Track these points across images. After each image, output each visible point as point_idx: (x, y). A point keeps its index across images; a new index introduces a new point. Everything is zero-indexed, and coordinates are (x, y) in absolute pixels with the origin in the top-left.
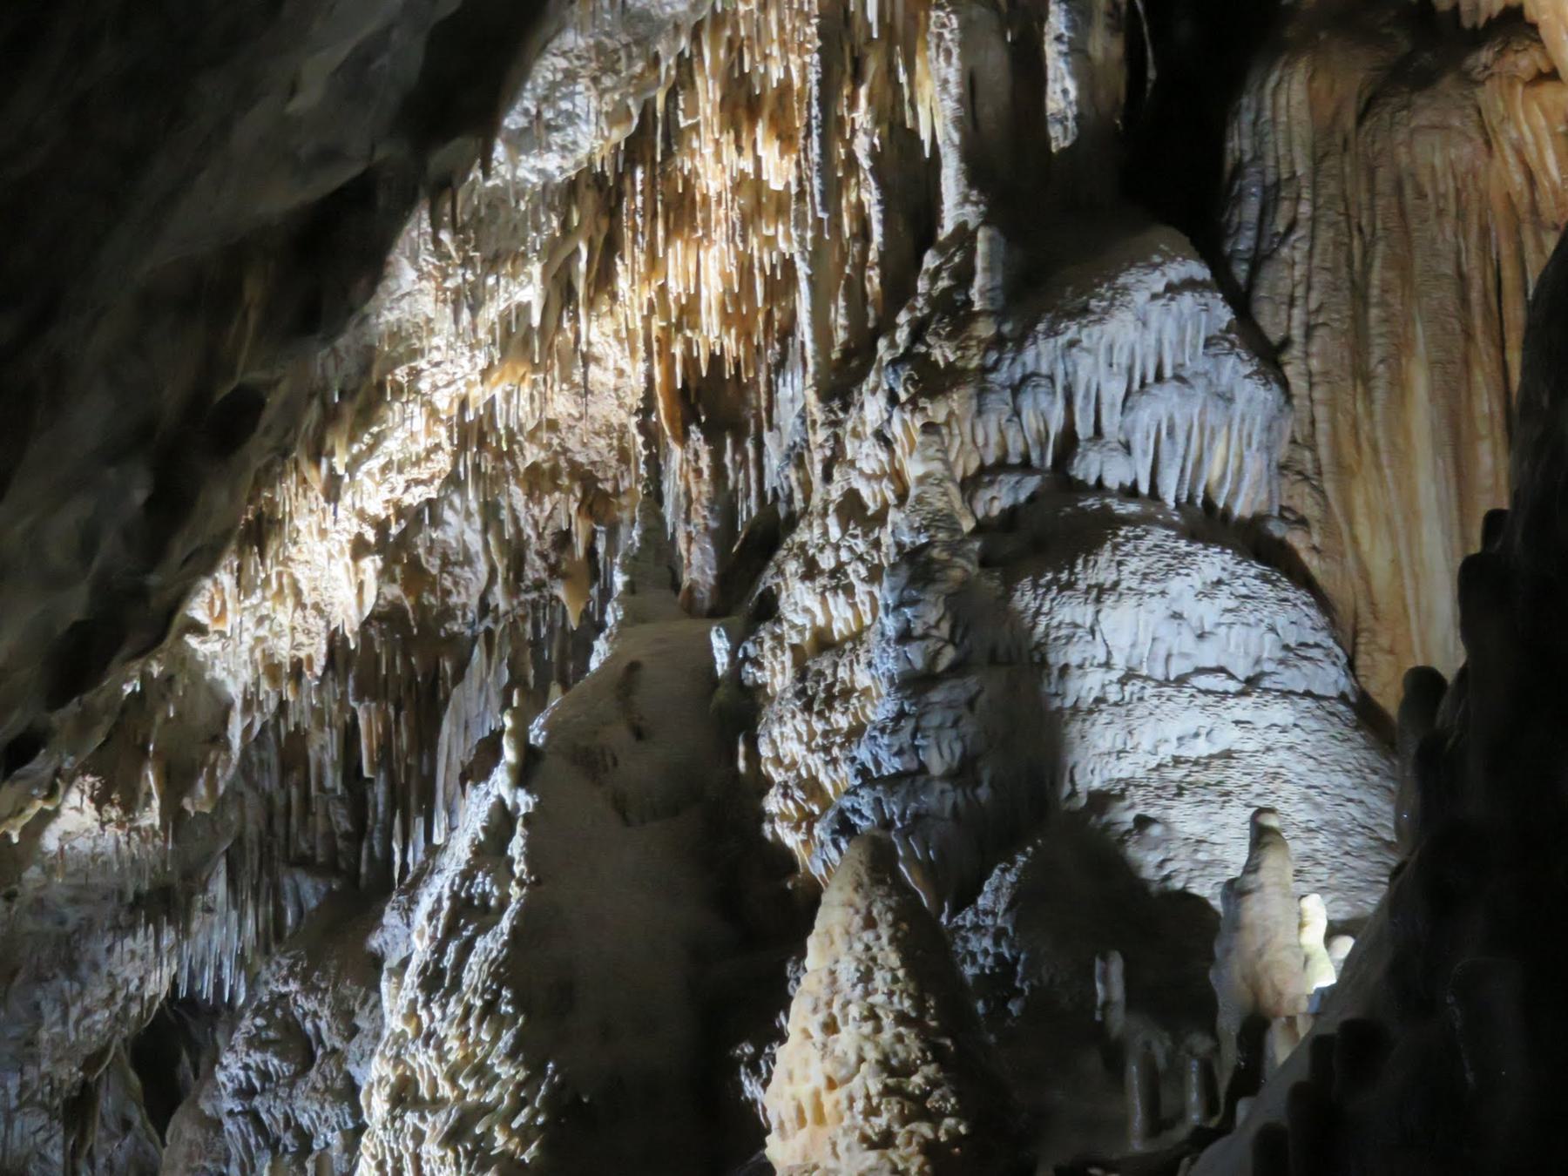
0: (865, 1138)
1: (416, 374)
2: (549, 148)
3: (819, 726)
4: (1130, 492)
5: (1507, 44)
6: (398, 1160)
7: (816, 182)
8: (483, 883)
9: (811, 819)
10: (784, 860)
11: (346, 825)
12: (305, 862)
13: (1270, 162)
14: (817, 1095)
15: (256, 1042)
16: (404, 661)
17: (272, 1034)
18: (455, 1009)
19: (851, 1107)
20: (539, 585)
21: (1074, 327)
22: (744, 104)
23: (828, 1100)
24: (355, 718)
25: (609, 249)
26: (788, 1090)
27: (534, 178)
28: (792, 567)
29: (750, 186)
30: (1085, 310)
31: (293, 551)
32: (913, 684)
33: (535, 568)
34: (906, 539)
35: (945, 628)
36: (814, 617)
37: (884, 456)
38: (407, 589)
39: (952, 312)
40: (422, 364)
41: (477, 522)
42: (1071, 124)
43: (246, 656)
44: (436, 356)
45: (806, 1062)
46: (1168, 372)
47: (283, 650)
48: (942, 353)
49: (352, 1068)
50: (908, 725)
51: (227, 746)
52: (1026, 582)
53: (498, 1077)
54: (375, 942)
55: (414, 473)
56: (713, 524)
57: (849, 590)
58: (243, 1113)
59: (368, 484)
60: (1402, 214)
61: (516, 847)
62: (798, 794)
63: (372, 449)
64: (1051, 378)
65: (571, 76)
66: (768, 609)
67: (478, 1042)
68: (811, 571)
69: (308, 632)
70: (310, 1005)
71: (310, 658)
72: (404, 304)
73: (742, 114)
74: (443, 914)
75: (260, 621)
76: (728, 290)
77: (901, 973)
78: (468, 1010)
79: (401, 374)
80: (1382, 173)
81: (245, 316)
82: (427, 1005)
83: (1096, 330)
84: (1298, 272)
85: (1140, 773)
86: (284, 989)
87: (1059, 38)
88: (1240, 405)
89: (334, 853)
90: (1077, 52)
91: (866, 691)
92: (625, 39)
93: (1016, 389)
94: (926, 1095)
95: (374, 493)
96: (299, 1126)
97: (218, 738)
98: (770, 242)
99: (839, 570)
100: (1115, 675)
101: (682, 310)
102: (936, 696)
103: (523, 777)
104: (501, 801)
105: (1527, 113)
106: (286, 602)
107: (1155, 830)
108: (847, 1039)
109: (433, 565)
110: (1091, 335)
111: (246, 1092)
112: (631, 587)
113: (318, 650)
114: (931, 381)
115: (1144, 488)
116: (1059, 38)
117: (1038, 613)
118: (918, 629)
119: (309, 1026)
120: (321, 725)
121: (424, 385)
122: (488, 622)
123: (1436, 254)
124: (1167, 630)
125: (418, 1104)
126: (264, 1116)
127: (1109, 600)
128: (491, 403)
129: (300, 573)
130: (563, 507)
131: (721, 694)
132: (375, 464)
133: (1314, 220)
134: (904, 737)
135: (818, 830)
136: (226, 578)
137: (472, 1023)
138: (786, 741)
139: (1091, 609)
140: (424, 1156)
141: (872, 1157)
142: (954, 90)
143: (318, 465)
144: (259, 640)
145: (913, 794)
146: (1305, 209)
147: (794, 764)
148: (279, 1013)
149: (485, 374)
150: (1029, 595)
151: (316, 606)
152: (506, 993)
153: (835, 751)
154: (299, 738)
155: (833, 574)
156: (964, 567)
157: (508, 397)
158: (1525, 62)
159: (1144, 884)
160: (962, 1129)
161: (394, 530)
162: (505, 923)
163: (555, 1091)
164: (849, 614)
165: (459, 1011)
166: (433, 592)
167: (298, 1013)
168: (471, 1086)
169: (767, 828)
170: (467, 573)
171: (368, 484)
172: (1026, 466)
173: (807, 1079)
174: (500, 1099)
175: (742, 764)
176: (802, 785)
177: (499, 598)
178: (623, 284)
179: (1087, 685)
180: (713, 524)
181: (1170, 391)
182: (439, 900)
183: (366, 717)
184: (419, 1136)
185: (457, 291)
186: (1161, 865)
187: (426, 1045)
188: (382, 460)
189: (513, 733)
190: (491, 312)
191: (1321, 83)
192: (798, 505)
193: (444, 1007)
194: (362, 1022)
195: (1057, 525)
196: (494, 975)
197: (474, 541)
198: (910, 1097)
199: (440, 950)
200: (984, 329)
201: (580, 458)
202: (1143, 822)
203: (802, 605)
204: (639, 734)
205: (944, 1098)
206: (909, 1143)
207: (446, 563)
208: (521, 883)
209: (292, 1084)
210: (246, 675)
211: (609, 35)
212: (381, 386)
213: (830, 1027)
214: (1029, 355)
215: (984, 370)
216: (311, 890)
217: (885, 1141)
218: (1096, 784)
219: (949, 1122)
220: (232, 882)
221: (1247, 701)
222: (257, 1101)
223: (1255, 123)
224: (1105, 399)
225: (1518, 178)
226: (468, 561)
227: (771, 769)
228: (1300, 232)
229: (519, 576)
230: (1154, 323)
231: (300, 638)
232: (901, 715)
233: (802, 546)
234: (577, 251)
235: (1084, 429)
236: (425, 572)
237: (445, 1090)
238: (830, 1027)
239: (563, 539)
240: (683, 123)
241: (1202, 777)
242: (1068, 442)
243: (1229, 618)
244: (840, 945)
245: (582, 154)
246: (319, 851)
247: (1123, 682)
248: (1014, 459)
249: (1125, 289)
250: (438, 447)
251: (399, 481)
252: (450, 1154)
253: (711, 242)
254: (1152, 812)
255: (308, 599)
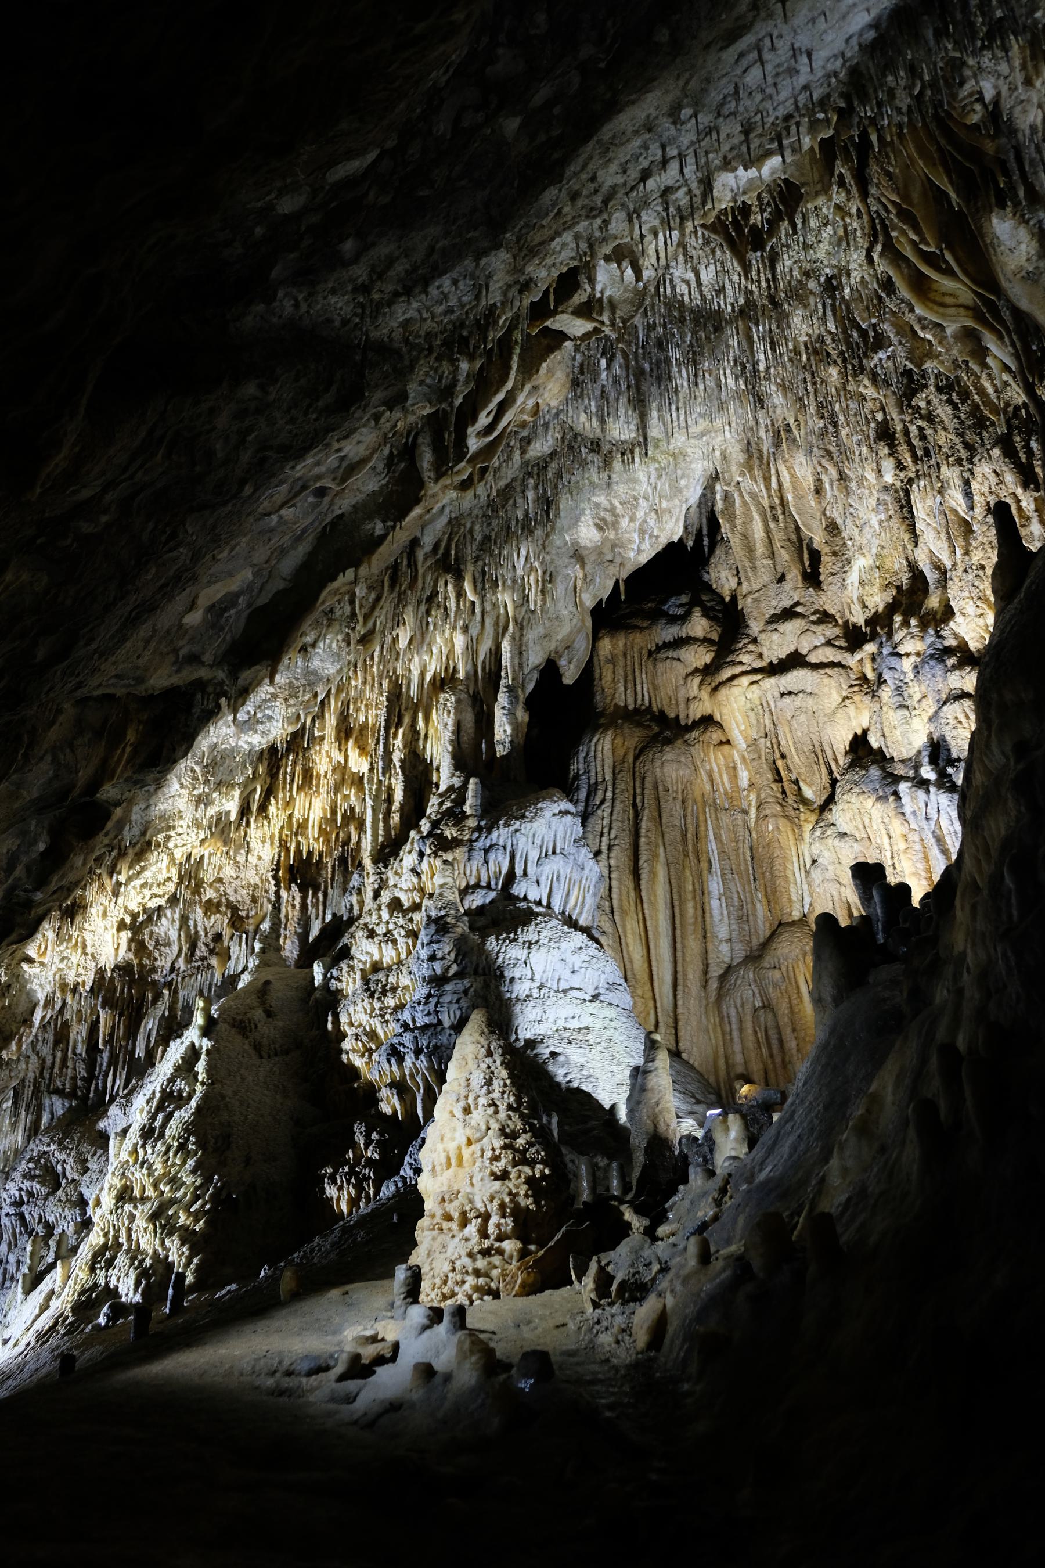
0: (493, 1174)
1: (168, 838)
2: (256, 732)
3: (377, 1005)
4: (539, 903)
5: (706, 729)
6: (117, 1231)
7: (381, 764)
8: (180, 1084)
9: (371, 1052)
10: (353, 1072)
11: (84, 1073)
12: (60, 1092)
13: (593, 774)
14: (459, 1149)
15: (27, 1176)
16: (130, 991)
17: (37, 1172)
18: (160, 1147)
19: (482, 1156)
20: (203, 959)
21: (518, 823)
22: (345, 731)
23: (466, 1153)
24: (98, 1017)
25: (269, 793)
26: (440, 1147)
27: (246, 746)
28: (360, 934)
29: (342, 769)
30: (523, 816)
31: (86, 925)
32: (437, 981)
33: (201, 950)
34: (433, 914)
35: (453, 955)
36: (372, 955)
37: (415, 880)
38: (136, 955)
39: (456, 816)
40: (172, 833)
41: (177, 925)
42: (507, 745)
43: (51, 978)
44: (179, 830)
45: (455, 1129)
46: (558, 851)
47: (71, 978)
48: (450, 832)
49: (84, 1190)
50: (433, 1001)
51: (31, 1026)
52: (493, 938)
53: (184, 1183)
54: (102, 1125)
55: (156, 890)
56: (299, 930)
57: (395, 942)
58: (15, 1215)
59: (133, 893)
60: (658, 799)
61: (201, 1067)
62: (364, 1038)
63: (139, 873)
64: (504, 847)
65: (274, 697)
66: (346, 953)
67: (174, 1164)
68: (372, 934)
69: (85, 968)
70: (63, 1156)
71: (84, 982)
72: (170, 801)
73: (343, 735)
74: (155, 1101)
75: (63, 959)
76: (324, 818)
77: (508, 1082)
78: (169, 1148)
79: (160, 837)
80: (647, 779)
81: (124, 749)
82: (143, 1146)
83: (529, 825)
84: (606, 821)
85: (549, 1033)
86: (46, 1149)
87: (504, 708)
88: (586, 872)
89: (74, 1087)
90: (511, 714)
91: (406, 987)
92: (303, 682)
93: (486, 851)
94: (526, 1150)
95: (134, 898)
96: (47, 1222)
97: (27, 1022)
98: (346, 797)
99: (388, 933)
100: (537, 984)
101: (299, 826)
102: (448, 987)
103: (206, 1031)
104: (193, 1044)
105: (716, 758)
106: (72, 955)
107: (561, 1058)
108: (478, 1117)
109: (150, 945)
110: (526, 827)
111: (18, 1203)
112: (263, 950)
113: (89, 978)
114: (443, 845)
115: (545, 903)
116: (504, 708)
117: (498, 952)
118: (439, 955)
119: (59, 1167)
120: (80, 1020)
121: (171, 845)
122: (173, 976)
123: (672, 816)
124: (559, 966)
125: (132, 1200)
126: (27, 1216)
127: (534, 948)
128: (202, 857)
129: (88, 936)
130: (220, 922)
131: (318, 994)
132: (137, 883)
133: (613, 799)
134: (431, 1006)
135: (375, 1056)
136: (51, 935)
137: (171, 1154)
138: (357, 1015)
139: (526, 951)
140: (134, 1228)
141: (498, 1184)
142: (450, 728)
143: (111, 877)
144: (60, 970)
145: (435, 1034)
146: (609, 794)
147: (360, 1025)
148: (42, 1161)
149: (203, 841)
150: (494, 943)
151: (93, 955)
152: (192, 1139)
153: (387, 1017)
154: (66, 1025)
155: (385, 935)
156: (463, 927)
157: (210, 855)
158: (716, 736)
159: (559, 1084)
160: (547, 1171)
161: (140, 919)
162: (193, 1103)
163: (217, 1192)
164: (394, 954)
165: (164, 1149)
166: (149, 958)
167: (54, 1161)
168: (167, 1188)
169: (344, 1057)
170: (167, 950)
171: (133, 893)
172: (488, 887)
173: (453, 1139)
174: (185, 1194)
175: (330, 1026)
176: (366, 1034)
177: (181, 964)
178: (272, 809)
179: (521, 989)
180: (299, 930)
181: (559, 858)
182: (154, 1093)
183: (104, 1016)
184: (132, 1217)
185: (200, 796)
186: (565, 1075)
187: (142, 1167)
188: (142, 881)
189: (203, 1009)
190: (212, 811)
191: (619, 740)
192: (356, 912)
193: (154, 1147)
194: (92, 1165)
195: (507, 914)
196: (186, 1130)
197: (173, 934)
198: (516, 1150)
199: (153, 1118)
200: (472, 823)
201: (232, 899)
202: (554, 1055)
203: (365, 950)
204: (269, 1014)
205: (538, 1152)
206: (519, 1177)
207: (157, 944)
208: (203, 1084)
209: (46, 1199)
210: (49, 988)
211: (297, 679)
212: (149, 843)
213: (467, 1110)
214: (495, 835)
215: (471, 841)
216: (60, 1106)
217: (504, 1176)
218: (528, 1036)
219: (539, 1167)
220: (15, 1104)
221: (594, 1004)
222: (24, 1208)
223: (585, 758)
224: (530, 859)
225: (708, 787)
226: (168, 944)
227: (347, 1028)
228: (608, 804)
229: (193, 954)
230: (553, 828)
231: (81, 971)
232: (429, 996)
233: (366, 924)
234: (255, 789)
235: (519, 871)
236: (146, 948)
237: (150, 1192)
238: (467, 1110)
239: (218, 938)
240: (317, 734)
241: (579, 1037)
242: (511, 877)
243: (585, 965)
244: (472, 1065)
245: (271, 737)
246: (67, 1086)
247: (540, 988)
248: (483, 884)
249: (542, 809)
250: (169, 879)
251: (148, 893)
252: (151, 1226)
253: (319, 793)
254: (557, 1050)
255: (89, 950)
